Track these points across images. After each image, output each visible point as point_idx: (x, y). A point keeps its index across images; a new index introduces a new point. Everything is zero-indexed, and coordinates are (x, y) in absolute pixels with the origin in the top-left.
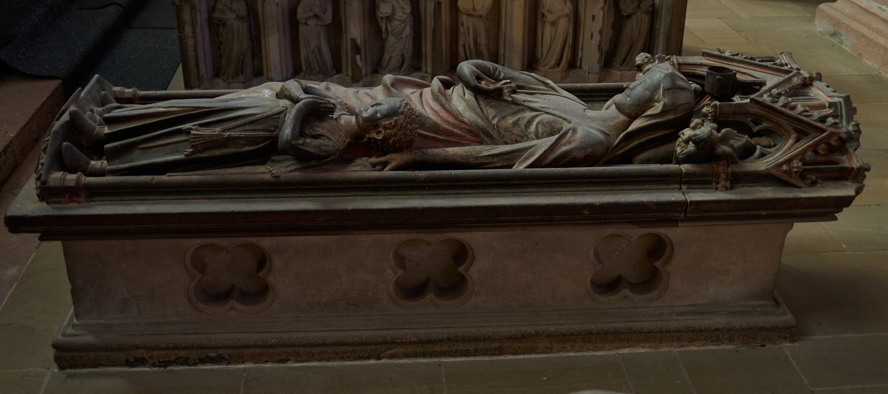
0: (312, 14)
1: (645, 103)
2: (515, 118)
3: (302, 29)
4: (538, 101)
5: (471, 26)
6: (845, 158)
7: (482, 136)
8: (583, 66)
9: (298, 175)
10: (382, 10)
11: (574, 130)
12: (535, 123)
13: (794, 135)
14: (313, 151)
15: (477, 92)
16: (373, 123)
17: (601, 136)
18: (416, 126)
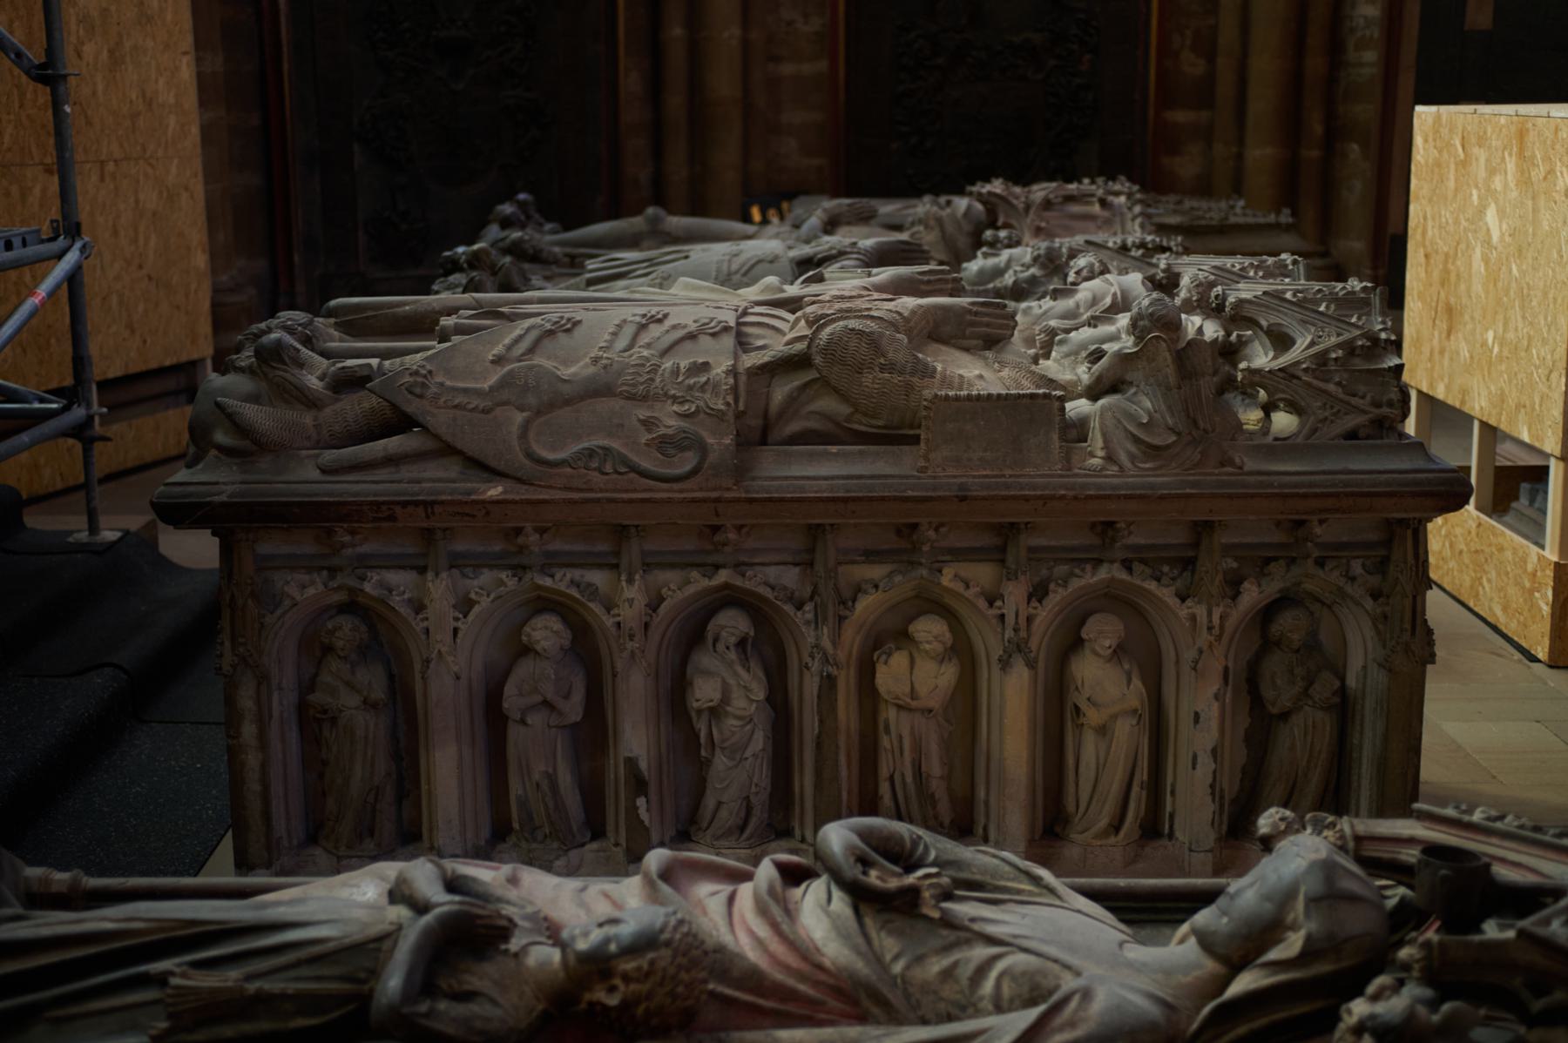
0: (538, 698)
2: (946, 962)
3: (515, 733)
4: (1005, 920)
5: (906, 733)
7: (866, 1003)
8: (1178, 834)
10: (698, 695)
11: (1087, 995)
12: (994, 974)
14: (450, 1030)
15: (860, 895)
16: (597, 965)
17: (1153, 1011)
18: (703, 975)
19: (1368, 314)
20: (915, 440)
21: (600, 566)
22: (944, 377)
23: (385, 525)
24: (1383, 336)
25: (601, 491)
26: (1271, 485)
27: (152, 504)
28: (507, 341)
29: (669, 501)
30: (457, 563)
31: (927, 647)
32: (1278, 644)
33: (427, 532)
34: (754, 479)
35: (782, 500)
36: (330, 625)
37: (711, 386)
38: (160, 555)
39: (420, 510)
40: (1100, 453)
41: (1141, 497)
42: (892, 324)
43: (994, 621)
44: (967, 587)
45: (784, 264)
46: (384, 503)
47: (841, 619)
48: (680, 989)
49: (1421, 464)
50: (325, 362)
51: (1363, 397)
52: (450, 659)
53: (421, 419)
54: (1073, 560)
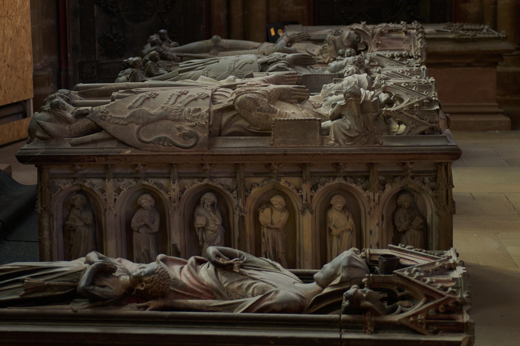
0: (143, 223)
1: (332, 276)
2: (239, 284)
3: (135, 236)
5: (270, 237)
6: (460, 316)
7: (215, 294)
9: (89, 311)
10: (197, 222)
11: (277, 292)
13: (424, 299)
14: (98, 294)
15: (218, 266)
19: (431, 91)
20: (269, 135)
21: (164, 178)
22: (280, 113)
23: (92, 163)
24: (434, 99)
25: (163, 152)
26: (391, 150)
27: (16, 156)
28: (133, 101)
29: (186, 155)
30: (116, 176)
31: (276, 206)
32: (401, 207)
33: (106, 165)
34: (214, 148)
35: (224, 155)
36: (73, 198)
37: (201, 117)
38: (13, 180)
39: (104, 158)
40: (333, 139)
41: (346, 154)
42: (264, 95)
43: (299, 198)
44: (290, 185)
45: (256, 65)
46: (91, 156)
47: (246, 196)
48: (161, 286)
49: (444, 143)
50: (74, 108)
51: (426, 120)
52: (113, 209)
53: (104, 128)
54: (326, 176)
